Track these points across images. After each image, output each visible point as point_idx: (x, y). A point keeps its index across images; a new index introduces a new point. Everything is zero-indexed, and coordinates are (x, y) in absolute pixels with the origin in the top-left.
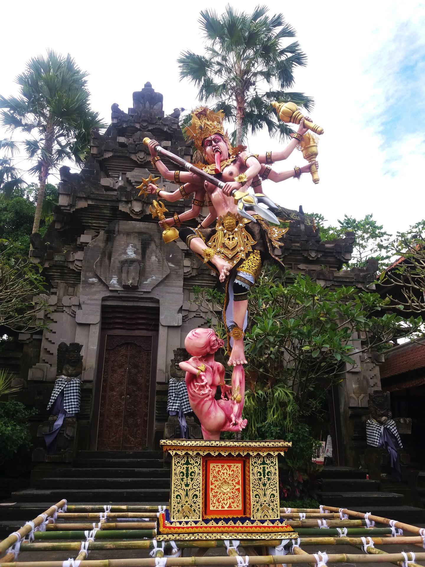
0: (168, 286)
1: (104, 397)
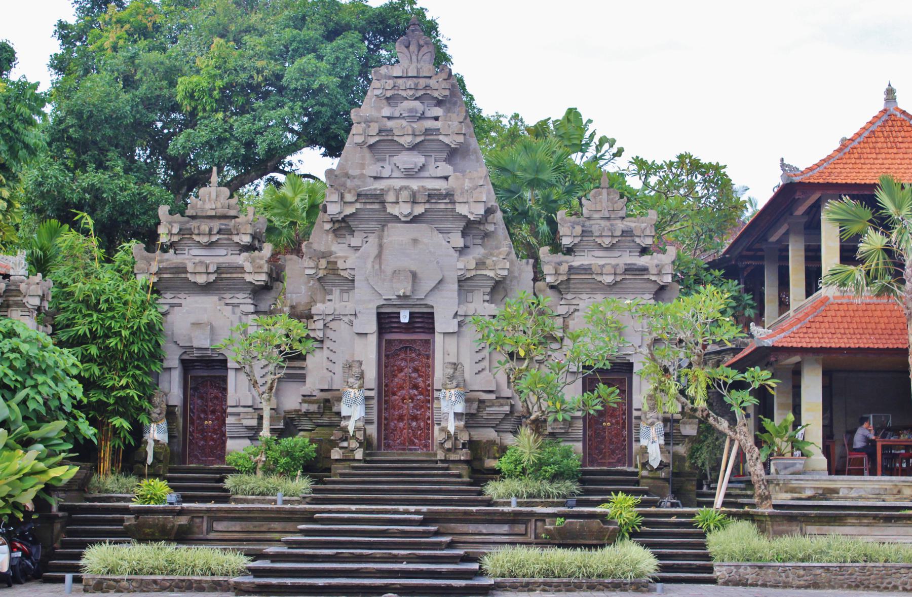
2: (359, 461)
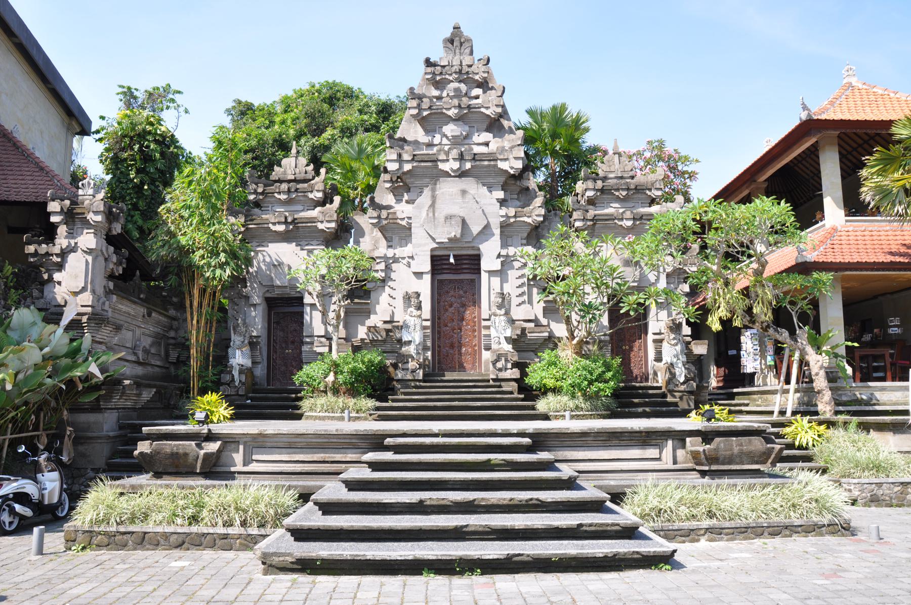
0: (487, 234)
1: (439, 332)
2: (419, 381)
